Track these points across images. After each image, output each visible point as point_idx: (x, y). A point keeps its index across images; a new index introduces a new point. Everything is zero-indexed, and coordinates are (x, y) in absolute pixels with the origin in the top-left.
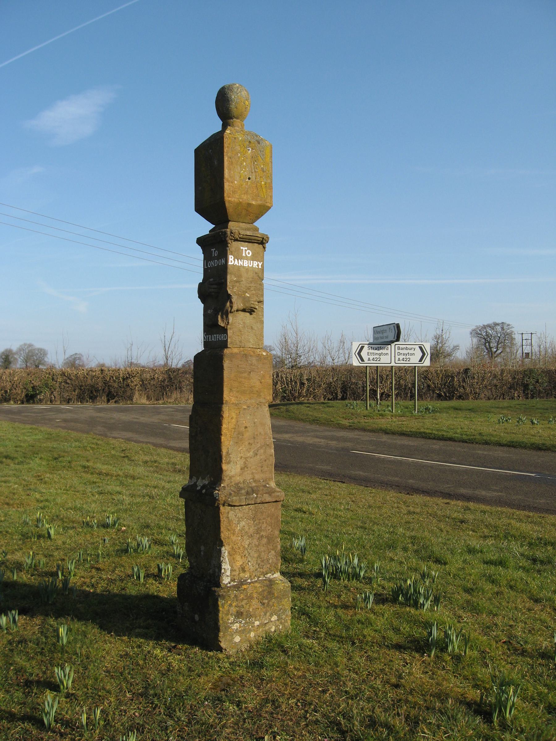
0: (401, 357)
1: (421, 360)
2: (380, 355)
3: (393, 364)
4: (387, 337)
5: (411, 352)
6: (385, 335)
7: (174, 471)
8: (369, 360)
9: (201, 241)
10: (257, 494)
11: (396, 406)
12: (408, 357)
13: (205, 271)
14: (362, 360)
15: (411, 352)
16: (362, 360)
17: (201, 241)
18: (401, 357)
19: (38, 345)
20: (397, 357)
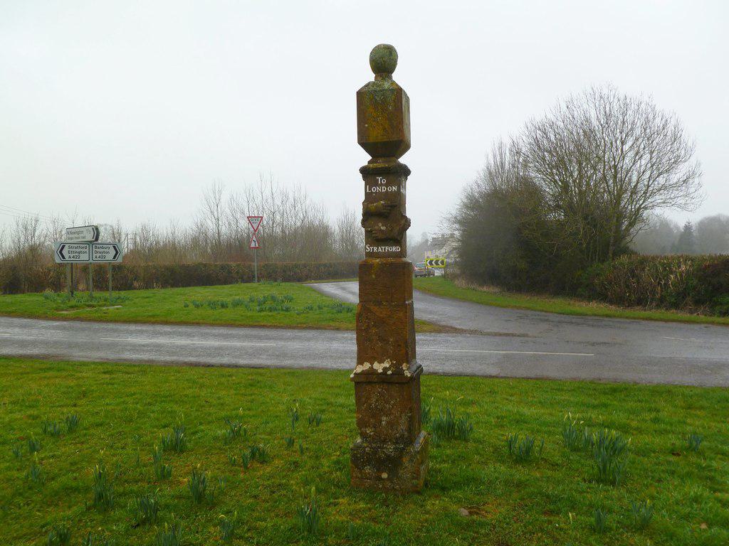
0: (98, 255)
1: (114, 258)
2: (79, 253)
3: (91, 261)
4: (84, 238)
5: (107, 250)
6: (82, 235)
7: (673, 454)
8: (70, 257)
9: (364, 171)
10: (388, 479)
11: (228, 300)
12: (103, 255)
13: (366, 194)
14: (64, 258)
15: (107, 250)
16: (64, 257)
17: (364, 171)
18: (98, 255)
19: (688, 137)
20: (94, 255)
